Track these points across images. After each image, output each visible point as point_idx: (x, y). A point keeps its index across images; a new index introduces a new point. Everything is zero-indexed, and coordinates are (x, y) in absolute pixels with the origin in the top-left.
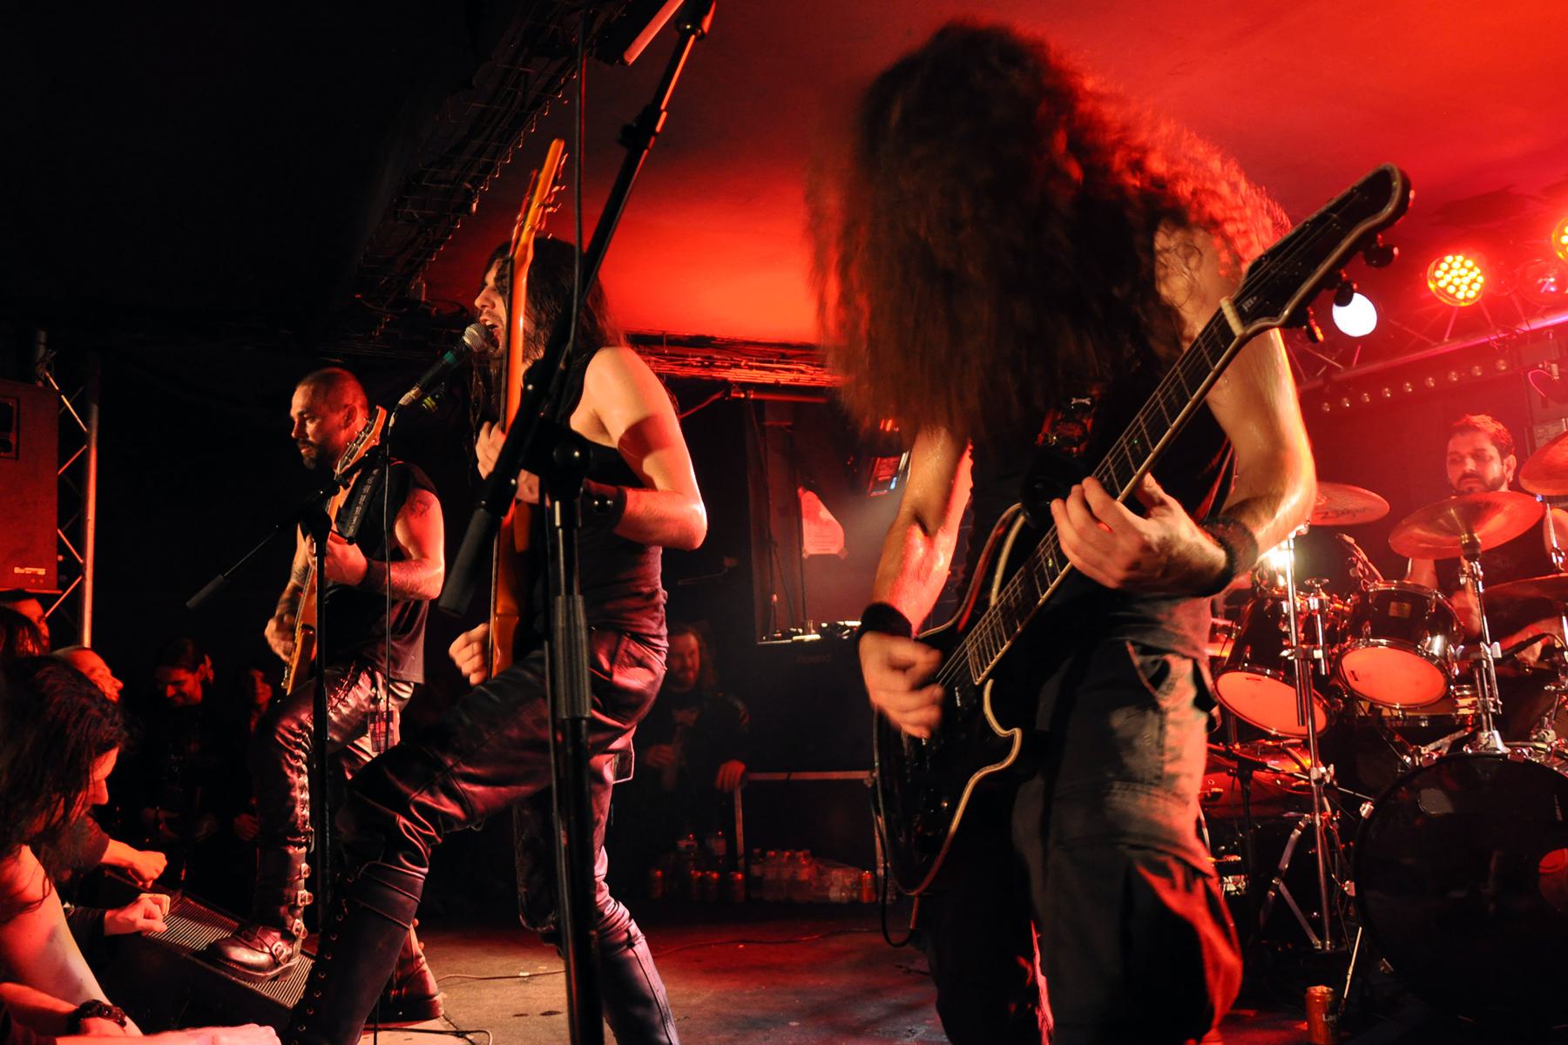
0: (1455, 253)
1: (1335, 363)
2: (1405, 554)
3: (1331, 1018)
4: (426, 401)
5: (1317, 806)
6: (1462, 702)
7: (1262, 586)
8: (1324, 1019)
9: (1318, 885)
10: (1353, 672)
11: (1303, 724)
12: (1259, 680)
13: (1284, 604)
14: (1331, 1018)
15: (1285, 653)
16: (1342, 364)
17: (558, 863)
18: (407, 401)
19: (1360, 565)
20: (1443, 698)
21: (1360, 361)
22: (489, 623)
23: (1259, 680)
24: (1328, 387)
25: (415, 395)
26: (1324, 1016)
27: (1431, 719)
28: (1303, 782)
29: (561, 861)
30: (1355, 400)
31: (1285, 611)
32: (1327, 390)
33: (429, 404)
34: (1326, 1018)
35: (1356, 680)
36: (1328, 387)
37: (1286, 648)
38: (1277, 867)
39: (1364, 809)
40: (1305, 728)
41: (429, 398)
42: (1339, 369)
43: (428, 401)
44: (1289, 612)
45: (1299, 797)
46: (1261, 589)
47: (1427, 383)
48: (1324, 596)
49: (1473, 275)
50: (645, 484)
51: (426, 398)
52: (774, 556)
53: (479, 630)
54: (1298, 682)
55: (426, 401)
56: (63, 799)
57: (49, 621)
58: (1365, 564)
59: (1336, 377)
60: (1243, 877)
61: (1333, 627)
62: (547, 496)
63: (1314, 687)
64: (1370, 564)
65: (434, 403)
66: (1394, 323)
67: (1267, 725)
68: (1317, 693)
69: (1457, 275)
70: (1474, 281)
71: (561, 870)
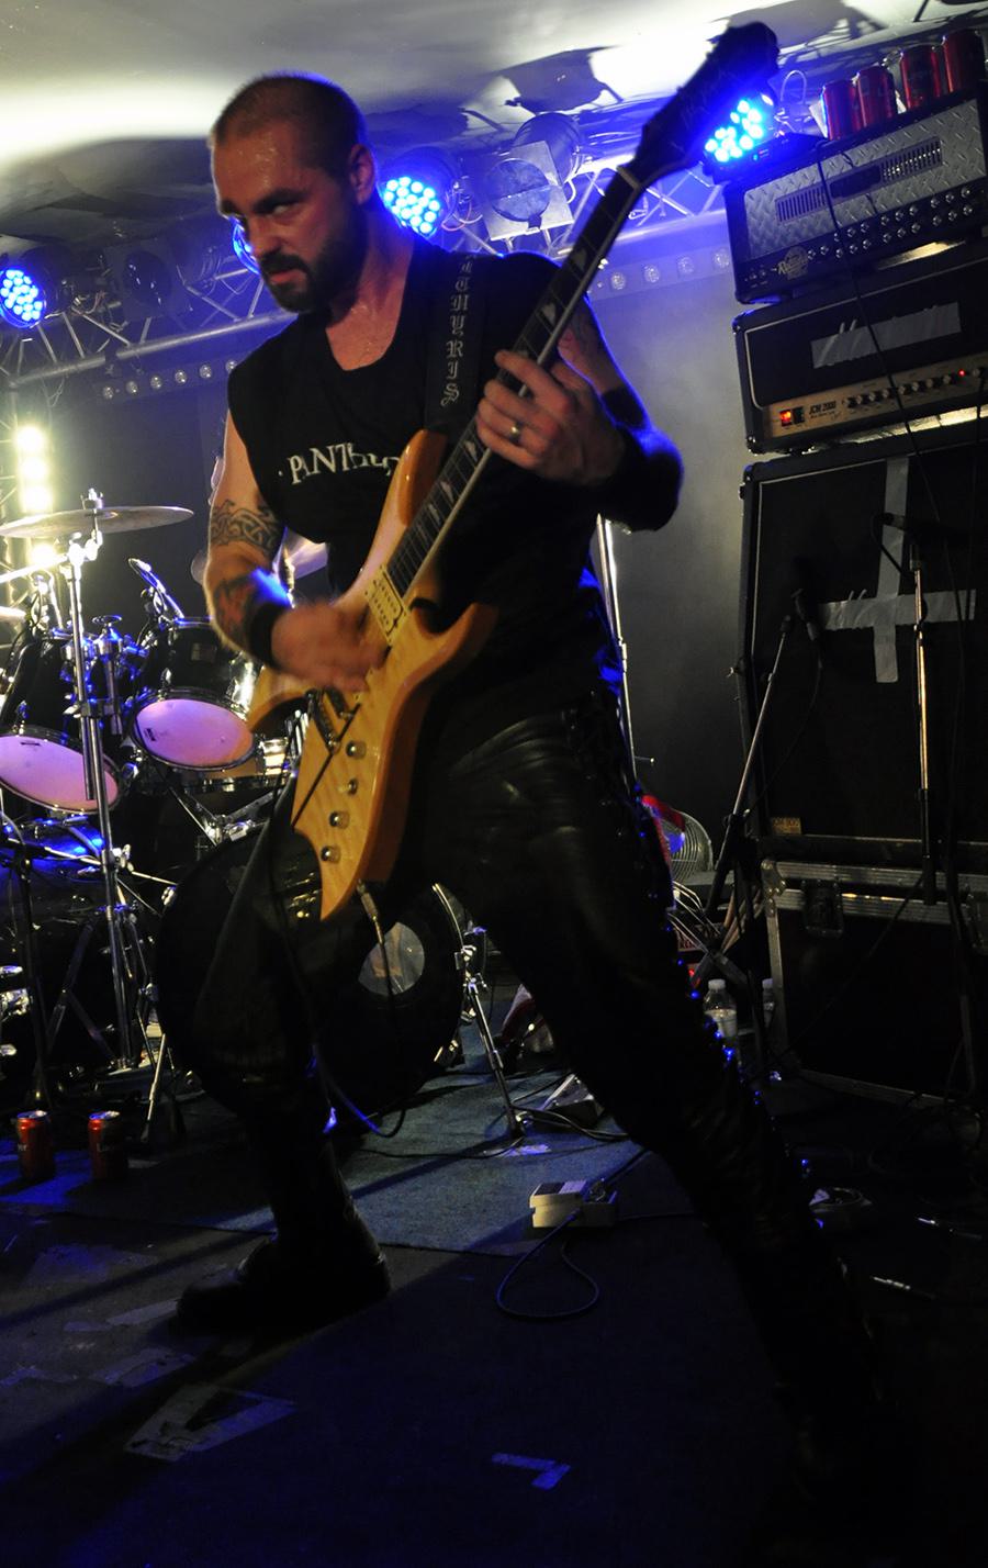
0: (397, 176)
1: (120, 338)
2: (637, 533)
3: (107, 1149)
5: (108, 897)
6: (270, 761)
7: (39, 626)
8: (98, 1150)
10: (149, 730)
11: (92, 798)
12: (38, 744)
13: (69, 649)
14: (107, 1149)
15: (70, 710)
16: (129, 340)
19: (157, 600)
20: (251, 756)
21: (149, 337)
23: (38, 744)
24: (112, 366)
26: (98, 1145)
27: (238, 782)
28: (91, 869)
30: (193, 375)
31: (69, 657)
32: (110, 371)
34: (101, 1148)
35: (153, 739)
36: (112, 366)
37: (70, 703)
39: (167, 896)
40: (94, 802)
42: (126, 345)
44: (74, 658)
45: (96, 886)
46: (38, 630)
47: (128, 389)
48: (114, 636)
49: (424, 202)
56: (111, 1101)
57: (120, 324)
58: (162, 597)
59: (122, 355)
60: (24, 991)
61: (126, 675)
63: (105, 752)
64: (169, 598)
66: (193, 291)
67: (47, 801)
68: (108, 759)
69: (405, 205)
70: (427, 209)
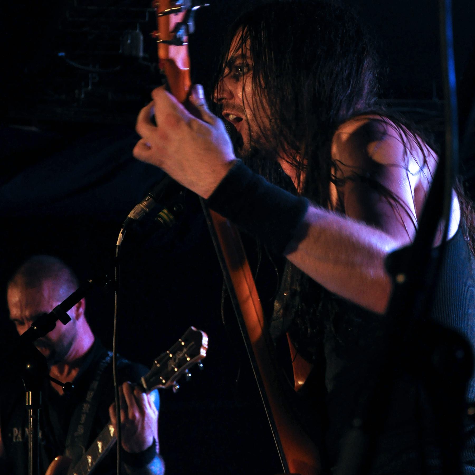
4: (161, 213)
9: (256, 380)
17: (29, 453)
18: (138, 214)
22: (115, 402)
25: (147, 206)
29: (30, 453)
33: (165, 217)
38: (191, 326)
41: (165, 211)
43: (164, 213)
50: (256, 138)
51: (161, 210)
52: (408, 136)
53: (113, 404)
54: (31, 445)
55: (161, 213)
62: (126, 230)
65: (171, 217)
71: (30, 455)
